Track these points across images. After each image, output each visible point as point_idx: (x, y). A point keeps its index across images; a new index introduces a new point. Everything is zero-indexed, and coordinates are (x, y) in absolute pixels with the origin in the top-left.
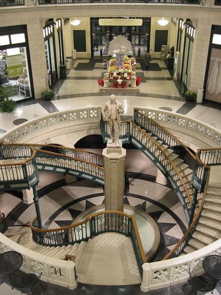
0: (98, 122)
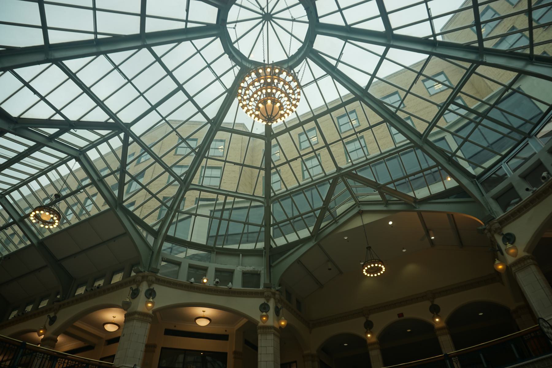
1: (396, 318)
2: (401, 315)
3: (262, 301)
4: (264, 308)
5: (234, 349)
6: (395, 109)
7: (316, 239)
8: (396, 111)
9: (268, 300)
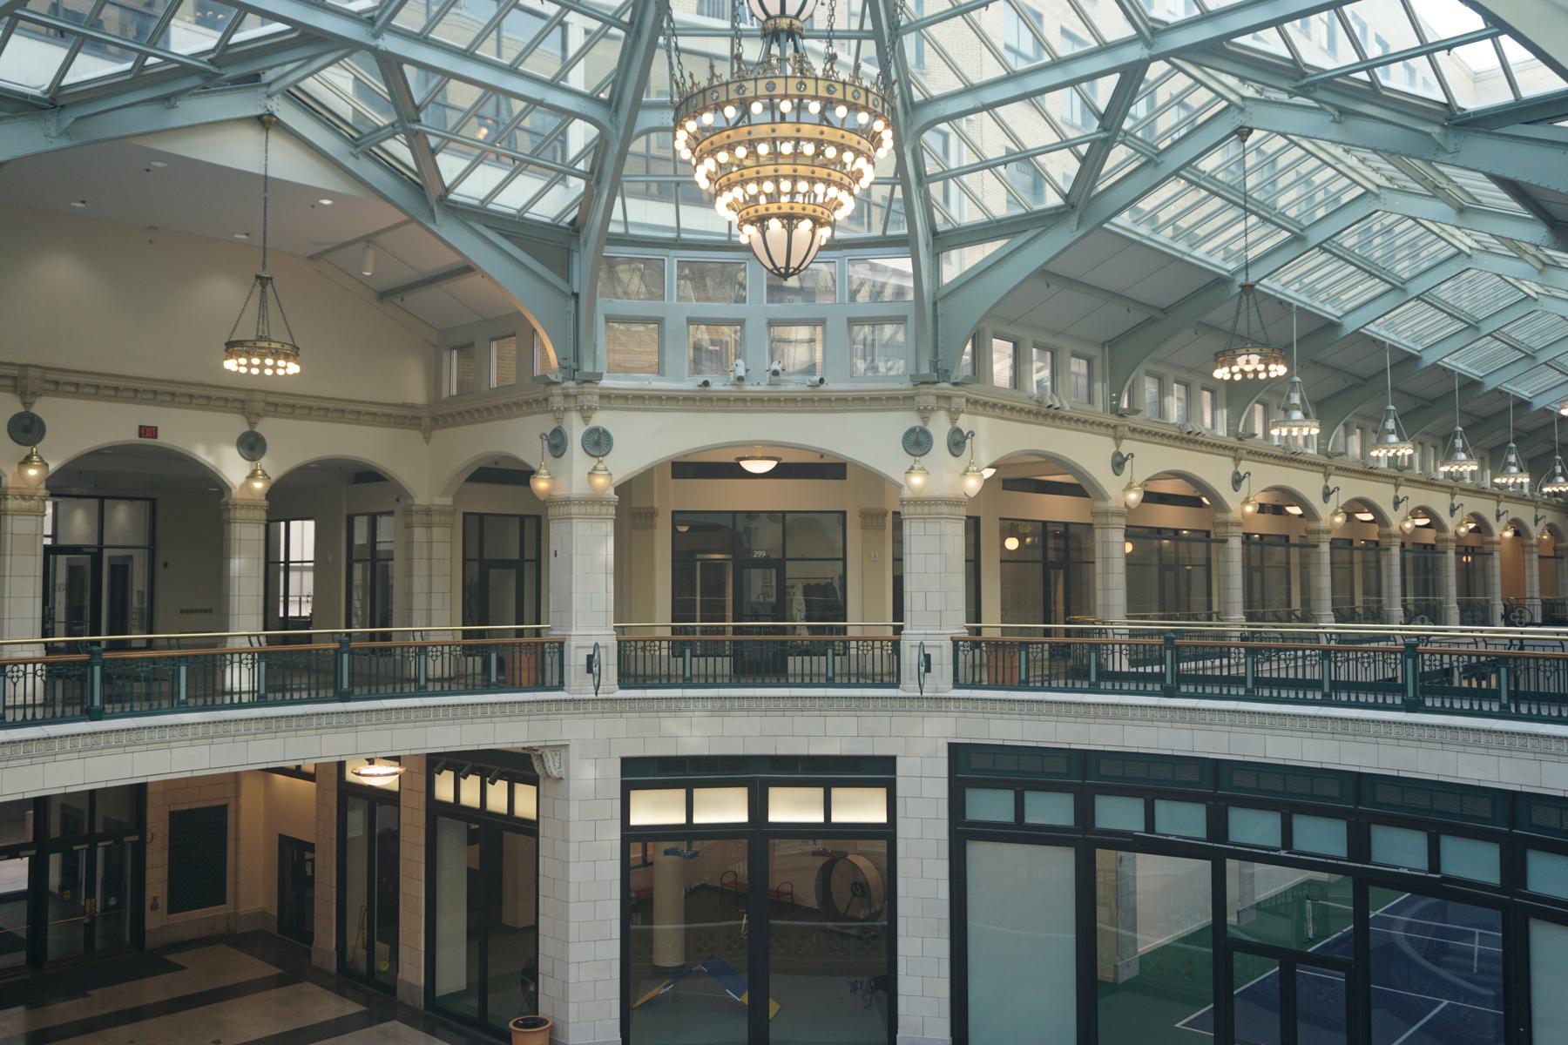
1: (131, 436)
2: (147, 431)
3: (910, 420)
4: (917, 442)
9: (925, 419)
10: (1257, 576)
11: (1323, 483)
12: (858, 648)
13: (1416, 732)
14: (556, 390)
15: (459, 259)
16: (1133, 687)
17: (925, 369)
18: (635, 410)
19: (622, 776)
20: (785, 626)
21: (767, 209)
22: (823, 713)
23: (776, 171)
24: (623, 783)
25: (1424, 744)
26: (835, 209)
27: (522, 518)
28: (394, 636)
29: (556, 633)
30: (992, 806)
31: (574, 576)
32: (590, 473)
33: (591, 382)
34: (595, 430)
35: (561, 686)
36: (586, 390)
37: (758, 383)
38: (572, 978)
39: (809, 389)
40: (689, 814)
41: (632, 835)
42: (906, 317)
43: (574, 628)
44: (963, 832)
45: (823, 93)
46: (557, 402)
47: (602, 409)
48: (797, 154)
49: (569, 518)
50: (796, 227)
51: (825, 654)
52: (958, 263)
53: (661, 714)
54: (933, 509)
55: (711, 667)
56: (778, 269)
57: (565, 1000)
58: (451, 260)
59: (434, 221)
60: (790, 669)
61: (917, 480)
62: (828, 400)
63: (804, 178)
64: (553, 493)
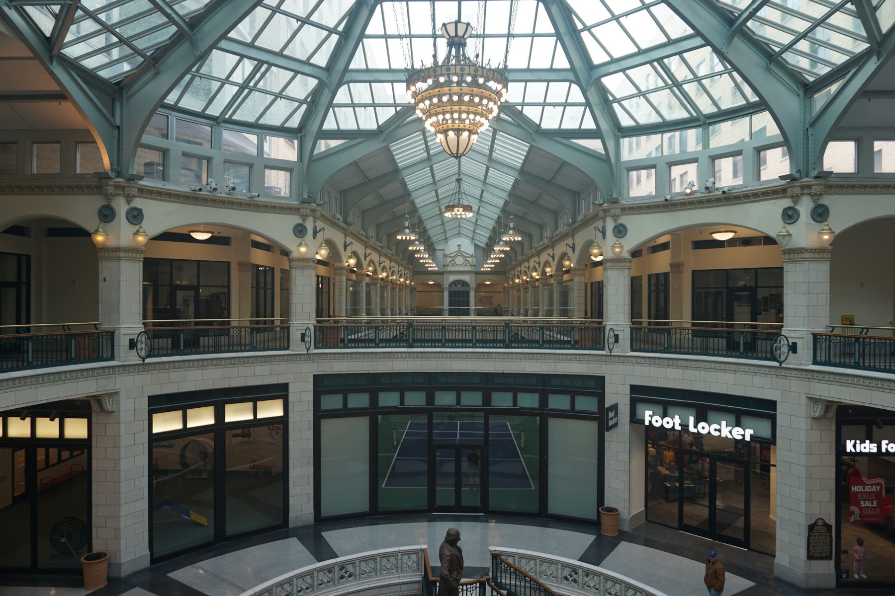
0: (418, 582)
3: (297, 220)
5: (670, 262)
6: (583, 27)
7: (385, 139)
8: (582, 30)
9: (304, 220)
10: (320, 296)
11: (313, 225)
12: (245, 332)
13: (510, 356)
14: (111, 182)
15: (59, 89)
16: (363, 345)
17: (305, 196)
18: (156, 199)
19: (149, 406)
20: (757, 324)
21: (459, 126)
22: (253, 364)
23: (451, 109)
24: (149, 410)
25: (513, 360)
26: (480, 126)
27: (19, 256)
28: (32, 330)
29: (105, 326)
30: (332, 402)
31: (121, 293)
32: (134, 234)
33: (133, 180)
34: (135, 209)
35: (112, 358)
36: (132, 185)
37: (221, 193)
38: (122, 525)
39: (249, 199)
40: (185, 423)
41: (155, 440)
42: (293, 169)
43: (121, 324)
44: (319, 415)
45: (472, 72)
46: (111, 190)
47: (138, 197)
48: (450, 101)
49: (118, 259)
50: (461, 135)
51: (664, 334)
52: (323, 146)
53: (170, 370)
54: (307, 264)
55: (716, 343)
56: (453, 154)
57: (117, 538)
58: (56, 88)
59: (51, 65)
60: (202, 343)
61: (303, 249)
62: (258, 206)
63: (464, 112)
64: (106, 244)
